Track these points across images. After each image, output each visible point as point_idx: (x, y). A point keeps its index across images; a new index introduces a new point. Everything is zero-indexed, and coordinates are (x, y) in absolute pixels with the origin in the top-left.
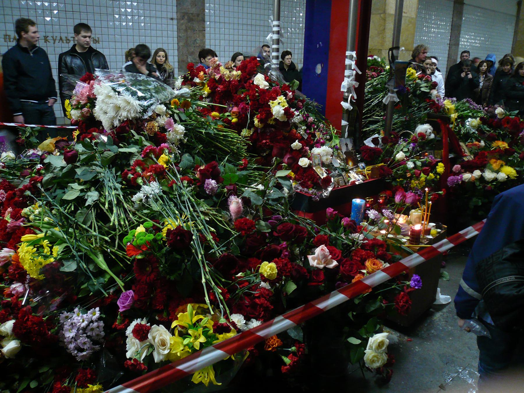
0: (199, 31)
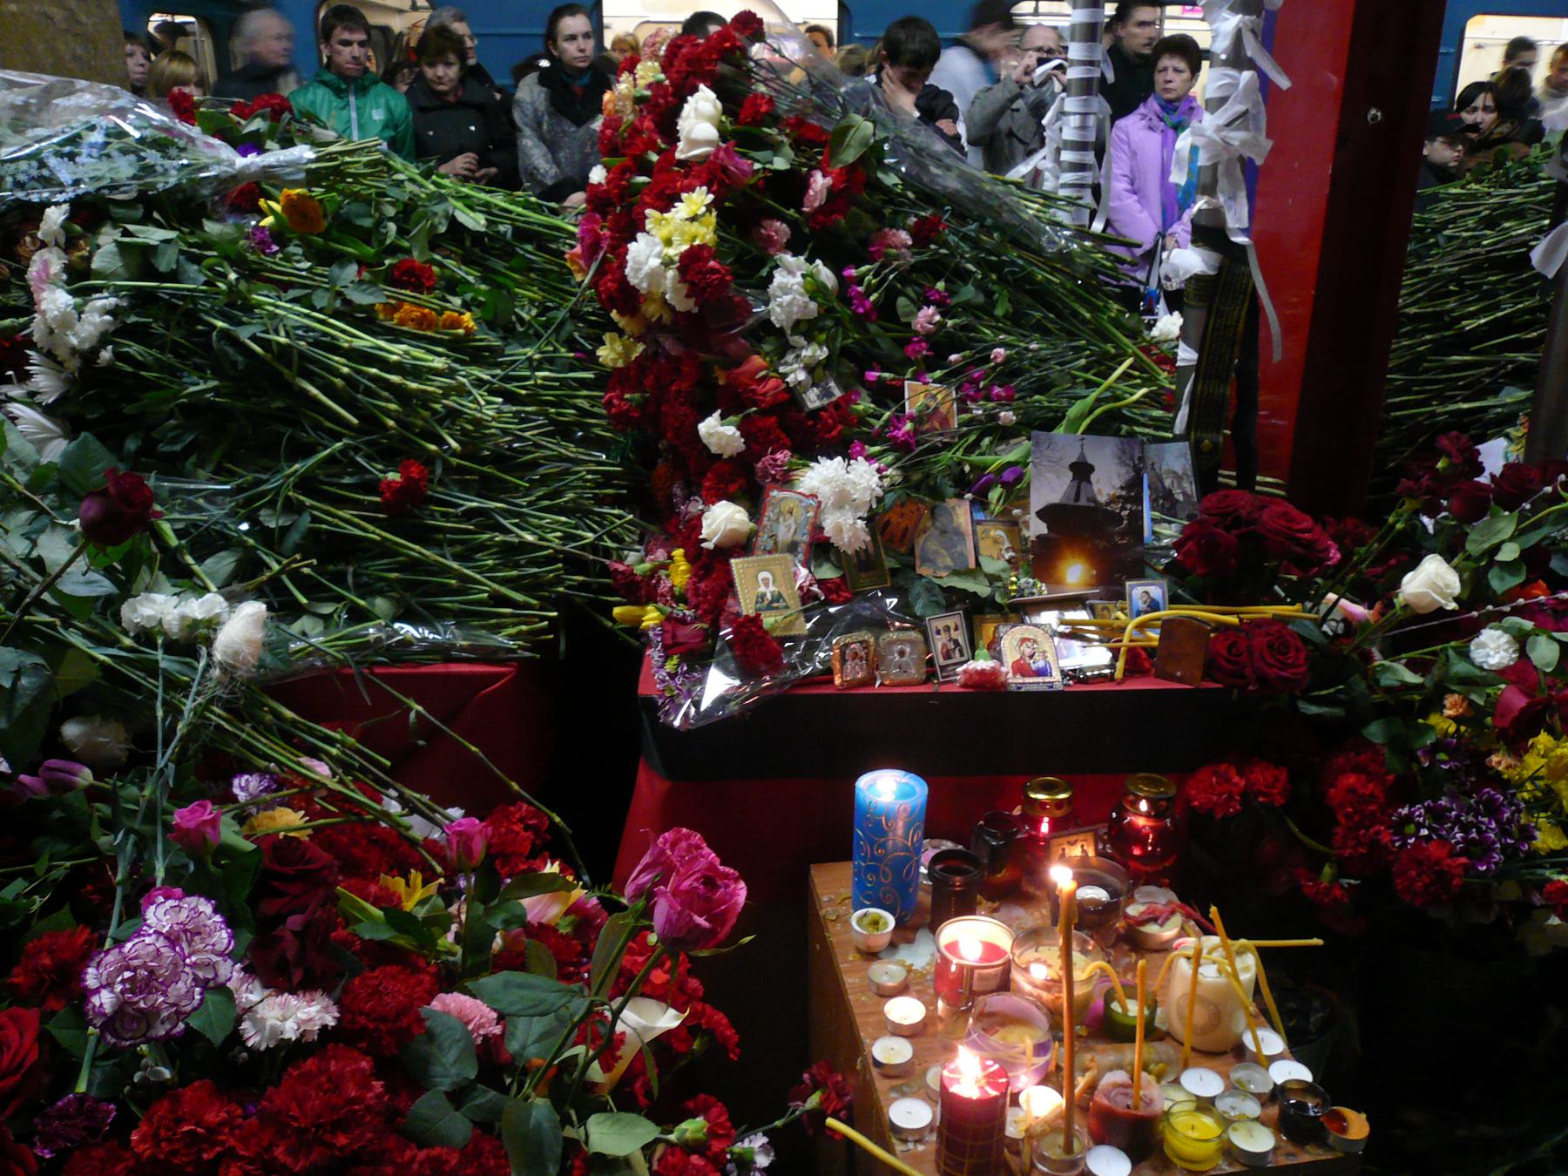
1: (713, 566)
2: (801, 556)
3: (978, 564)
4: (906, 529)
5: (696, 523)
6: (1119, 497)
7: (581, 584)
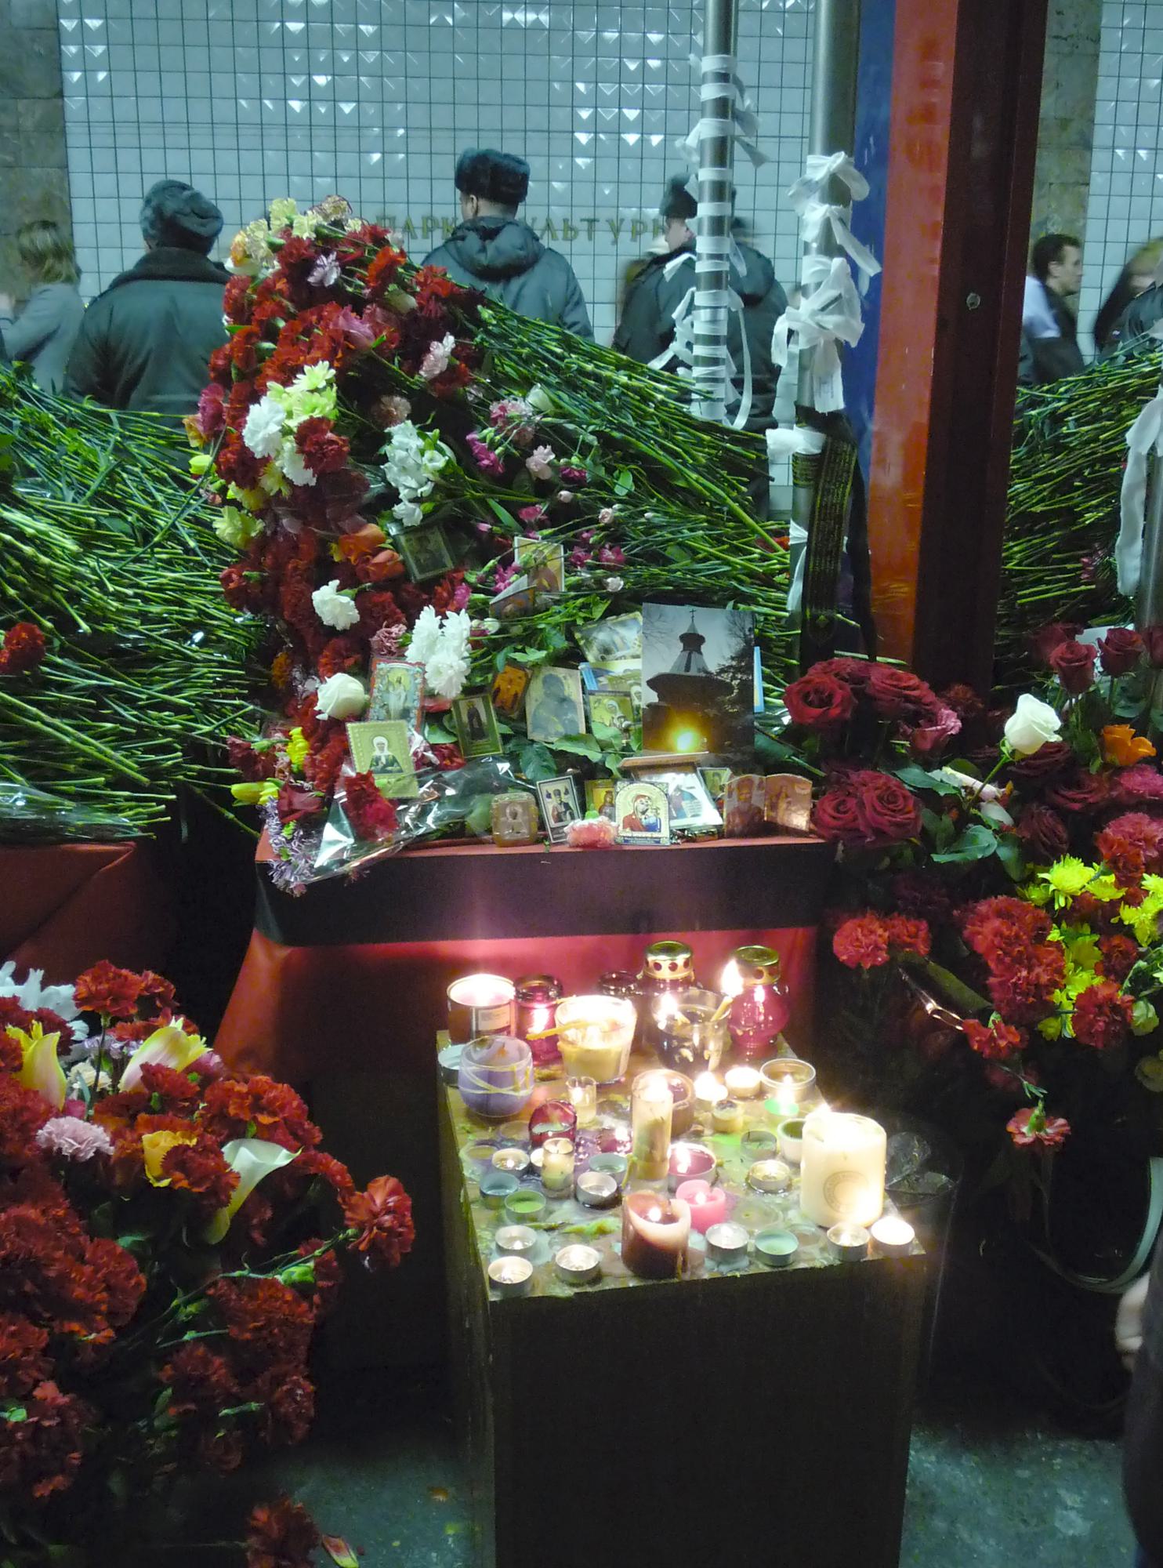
0: (1064, 185)
1: (330, 736)
2: (414, 721)
3: (589, 730)
4: (516, 695)
5: (312, 699)
6: (730, 667)
7: (200, 772)
